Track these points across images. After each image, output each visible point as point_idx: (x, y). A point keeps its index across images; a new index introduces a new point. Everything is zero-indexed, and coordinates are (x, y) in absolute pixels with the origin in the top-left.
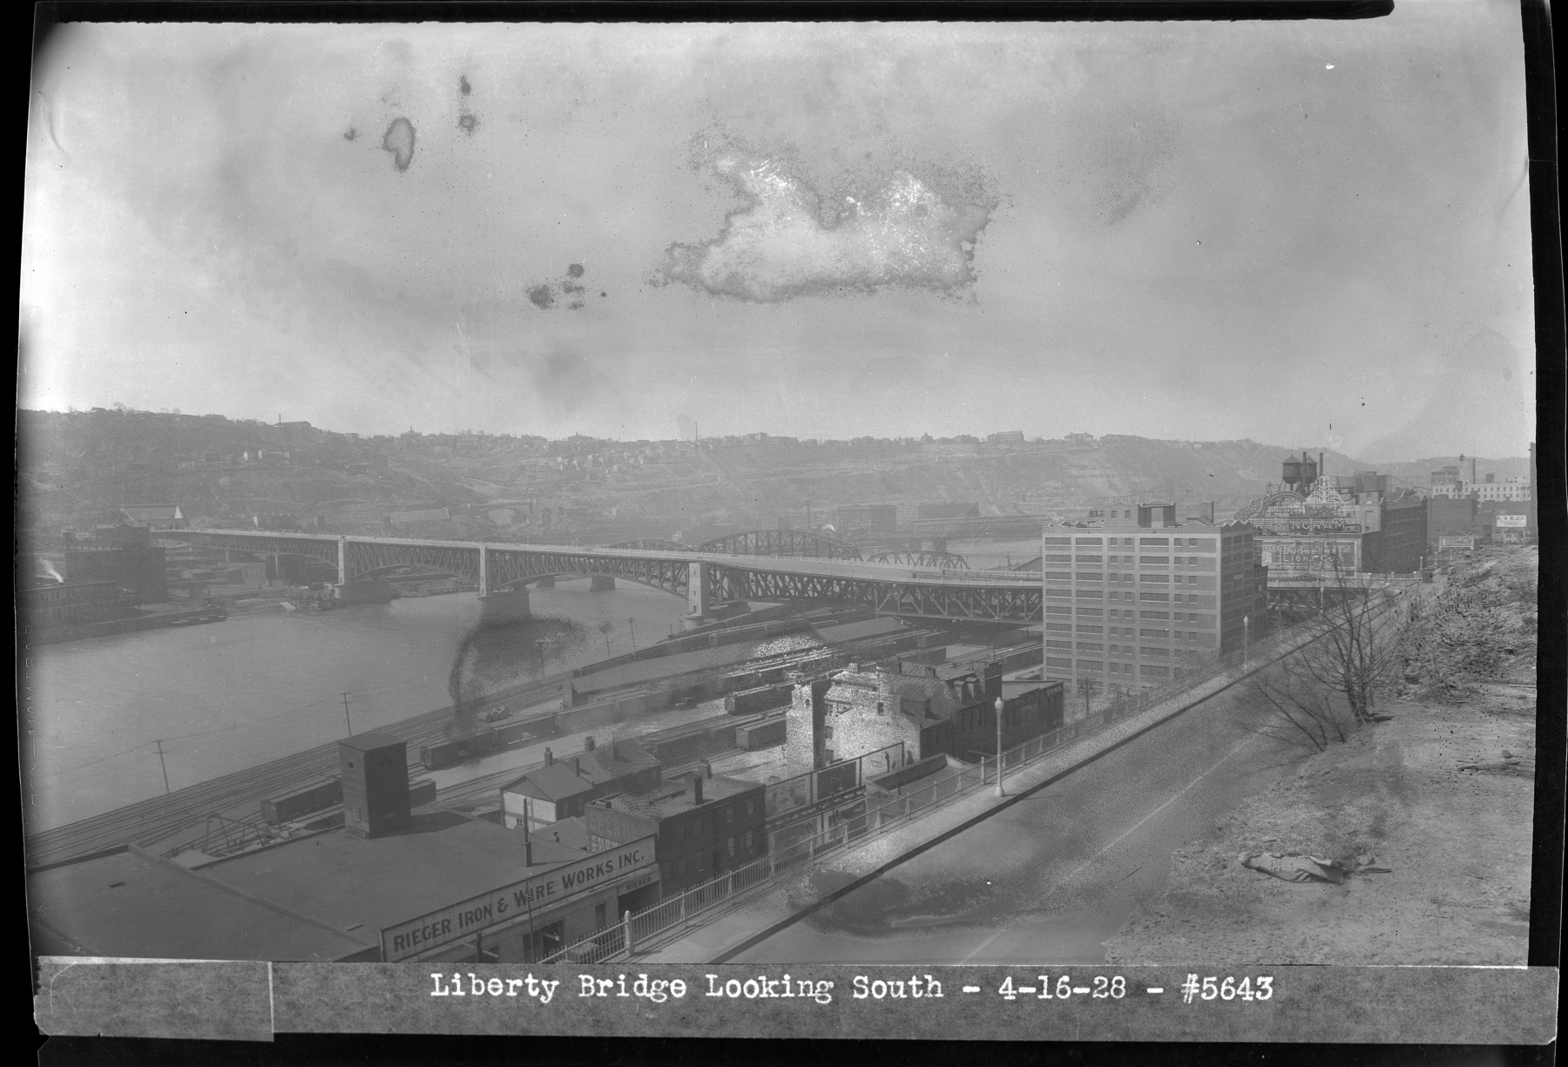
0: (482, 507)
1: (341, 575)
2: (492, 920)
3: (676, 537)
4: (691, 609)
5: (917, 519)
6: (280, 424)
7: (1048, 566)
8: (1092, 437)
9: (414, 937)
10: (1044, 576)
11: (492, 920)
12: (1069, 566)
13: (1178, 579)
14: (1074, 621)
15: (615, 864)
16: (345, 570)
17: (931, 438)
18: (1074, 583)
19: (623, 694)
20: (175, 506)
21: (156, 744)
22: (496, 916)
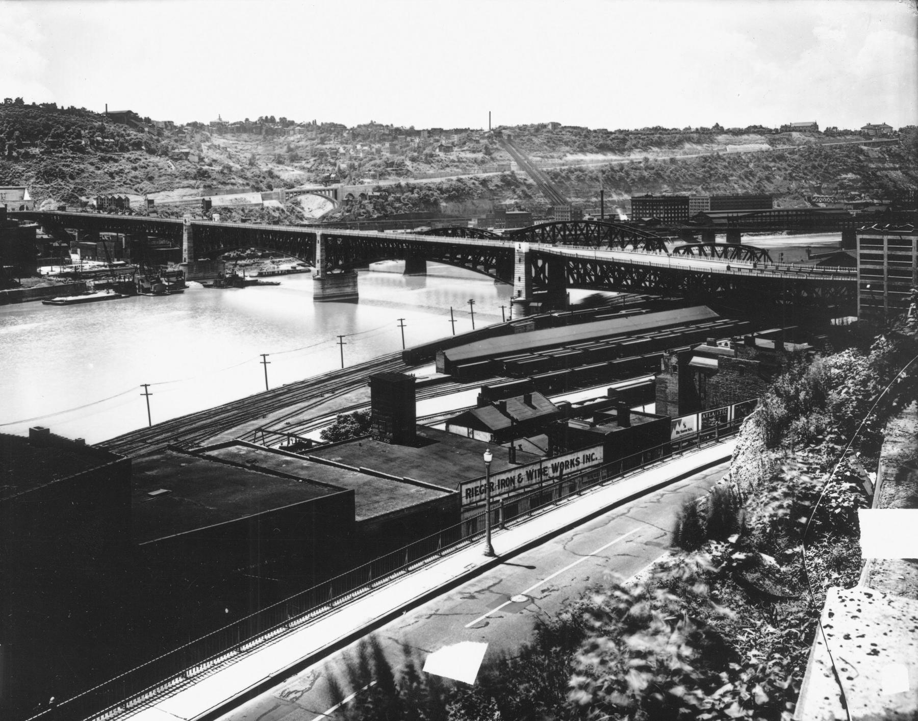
0: (292, 193)
1: (185, 255)
2: (514, 487)
3: (472, 224)
4: (515, 294)
5: (709, 211)
6: (107, 113)
7: (862, 263)
8: (891, 128)
9: (476, 491)
10: (858, 272)
11: (514, 487)
12: (882, 249)
13: (890, 257)
14: (885, 267)
15: (581, 460)
16: (189, 251)
17: (722, 128)
18: (885, 264)
19: (150, 454)
20: (24, 189)
21: (144, 387)
22: (517, 485)
